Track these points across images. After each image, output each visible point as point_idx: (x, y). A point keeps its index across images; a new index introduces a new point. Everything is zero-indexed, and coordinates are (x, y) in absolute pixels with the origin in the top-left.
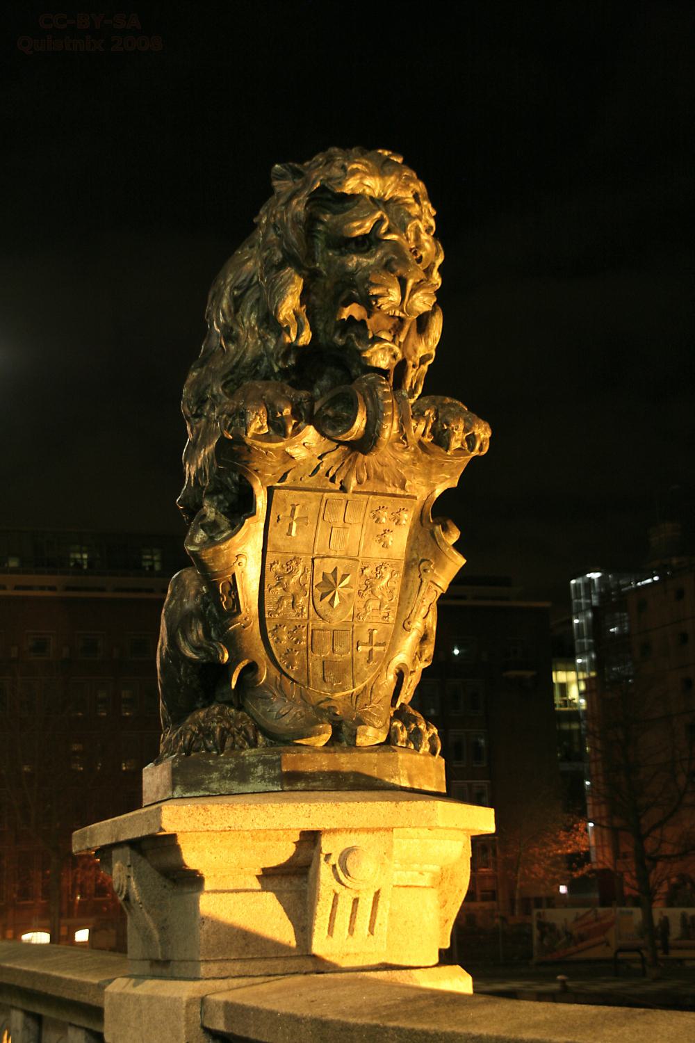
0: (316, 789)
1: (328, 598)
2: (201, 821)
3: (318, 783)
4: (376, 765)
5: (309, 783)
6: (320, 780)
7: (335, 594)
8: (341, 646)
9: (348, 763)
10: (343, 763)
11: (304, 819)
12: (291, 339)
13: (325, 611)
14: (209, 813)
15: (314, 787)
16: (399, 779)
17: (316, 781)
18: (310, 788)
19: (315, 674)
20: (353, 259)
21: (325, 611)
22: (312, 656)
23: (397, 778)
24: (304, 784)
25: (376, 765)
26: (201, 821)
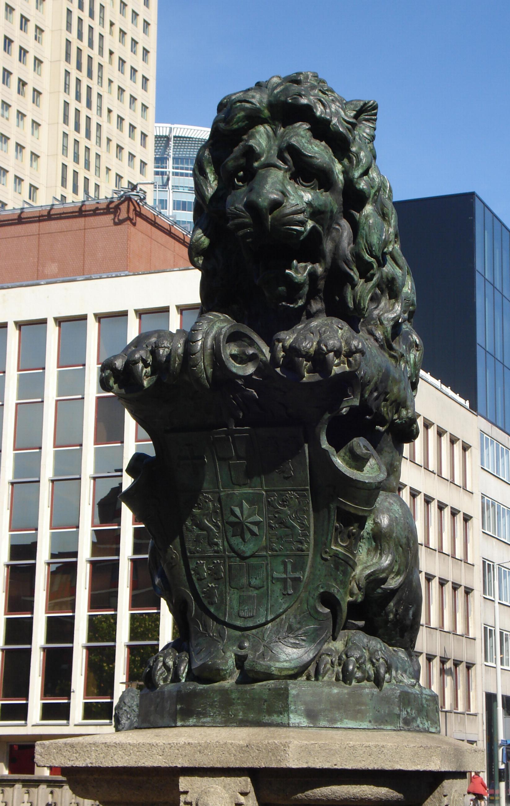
0: (206, 725)
1: (255, 529)
2: (67, 757)
3: (208, 719)
4: (266, 701)
5: (200, 718)
6: (210, 716)
7: (247, 526)
8: (256, 579)
9: (238, 699)
10: (234, 699)
11: (158, 757)
12: (202, 236)
13: (238, 544)
14: (74, 749)
15: (204, 723)
16: (288, 715)
17: (206, 717)
18: (200, 724)
19: (231, 608)
20: (258, 132)
21: (238, 544)
22: (230, 590)
23: (286, 715)
24: (195, 720)
25: (266, 701)
26: (67, 757)
